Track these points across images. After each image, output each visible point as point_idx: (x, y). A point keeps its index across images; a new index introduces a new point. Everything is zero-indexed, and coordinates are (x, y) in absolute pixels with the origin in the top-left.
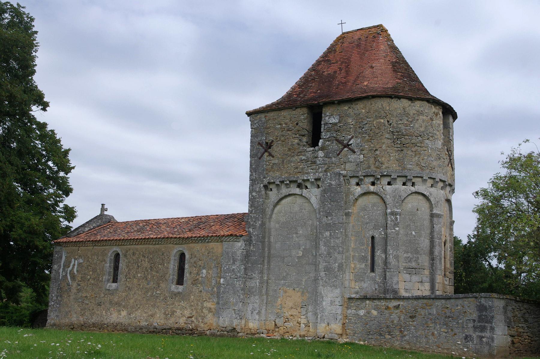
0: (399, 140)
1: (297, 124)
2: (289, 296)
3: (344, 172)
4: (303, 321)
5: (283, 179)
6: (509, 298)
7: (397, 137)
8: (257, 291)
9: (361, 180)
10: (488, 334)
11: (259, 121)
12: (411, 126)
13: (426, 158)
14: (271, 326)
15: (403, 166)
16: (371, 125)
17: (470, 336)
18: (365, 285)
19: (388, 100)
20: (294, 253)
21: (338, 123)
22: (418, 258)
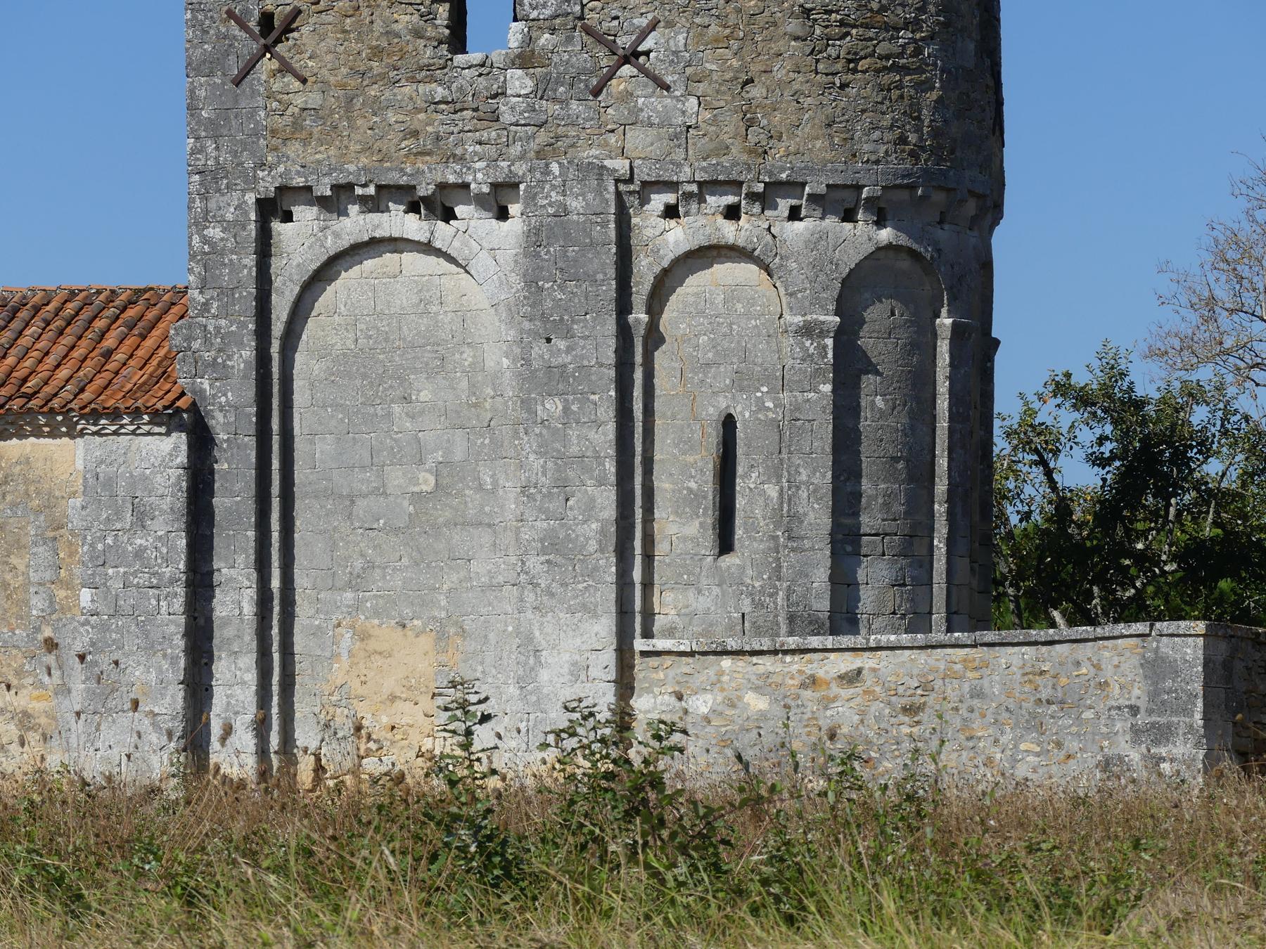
2: (380, 653)
5: (351, 178)
17: (1120, 758)
20: (396, 478)
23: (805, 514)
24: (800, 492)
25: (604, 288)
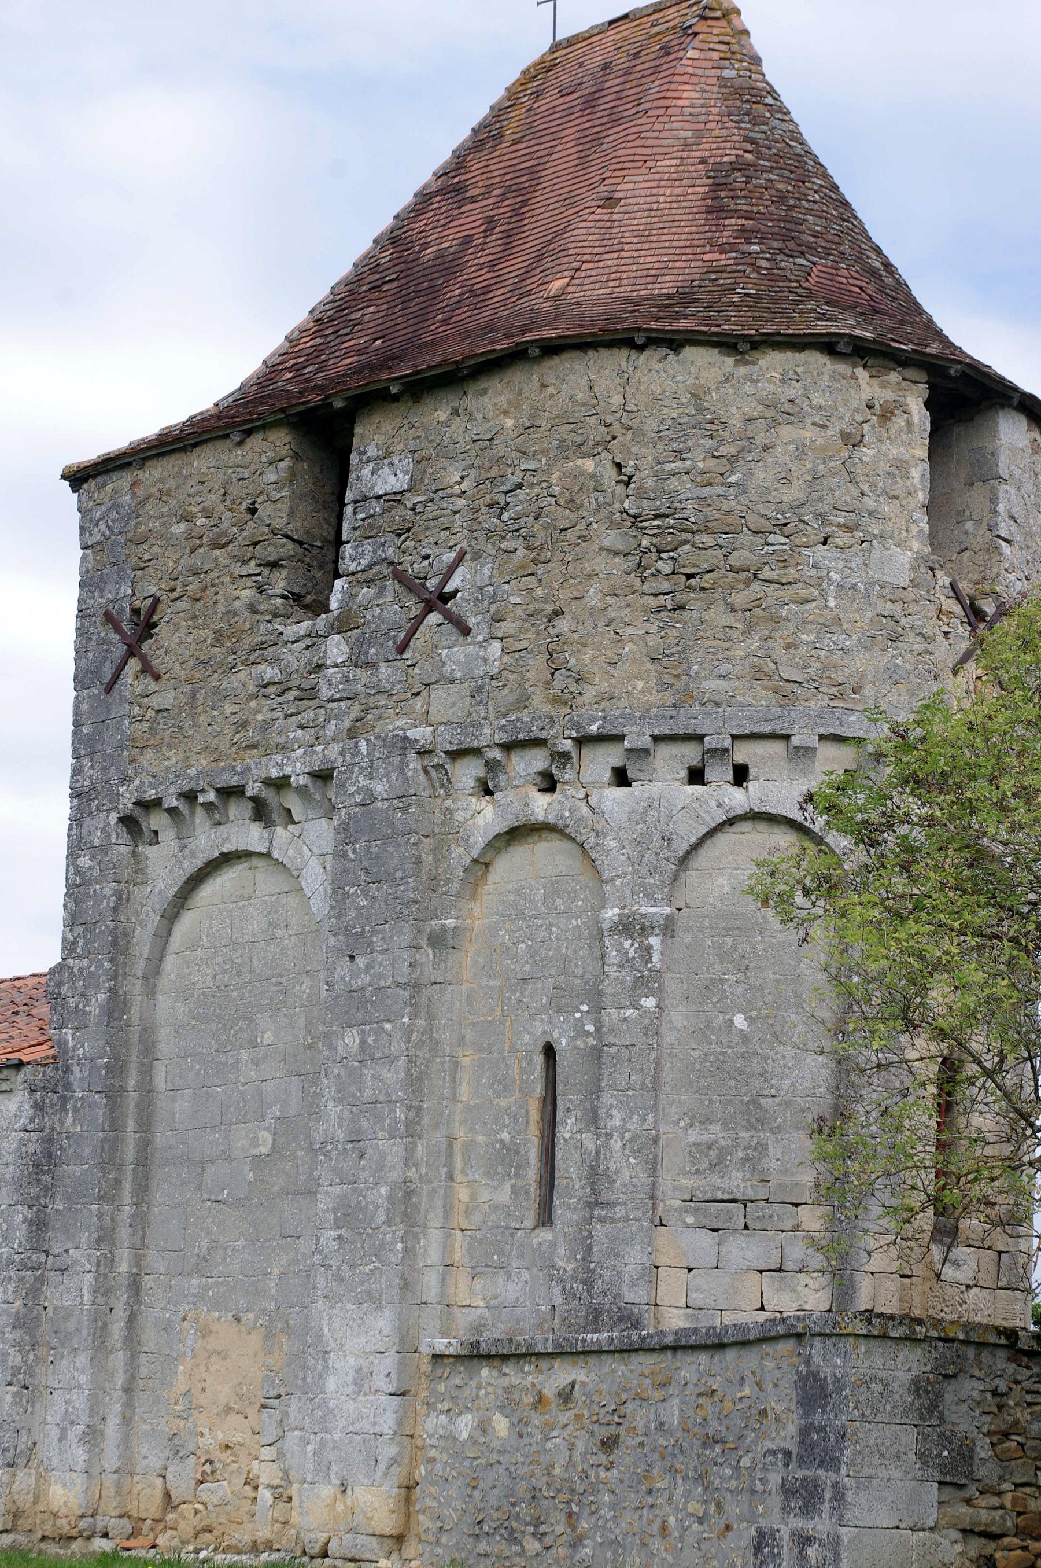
0: (664, 555)
1: (252, 511)
2: (219, 1353)
3: (421, 734)
4: (267, 1473)
5: (193, 785)
6: (961, 1336)
7: (655, 540)
8: (85, 1332)
9: (492, 766)
10: (821, 1525)
11: (109, 509)
12: (733, 479)
13: (812, 637)
14: (149, 1503)
15: (679, 684)
16: (537, 490)
18: (510, 1291)
19: (621, 357)
21: (409, 490)
22: (762, 1148)
23: (617, 1172)
24: (612, 1142)
25: (402, 888)
